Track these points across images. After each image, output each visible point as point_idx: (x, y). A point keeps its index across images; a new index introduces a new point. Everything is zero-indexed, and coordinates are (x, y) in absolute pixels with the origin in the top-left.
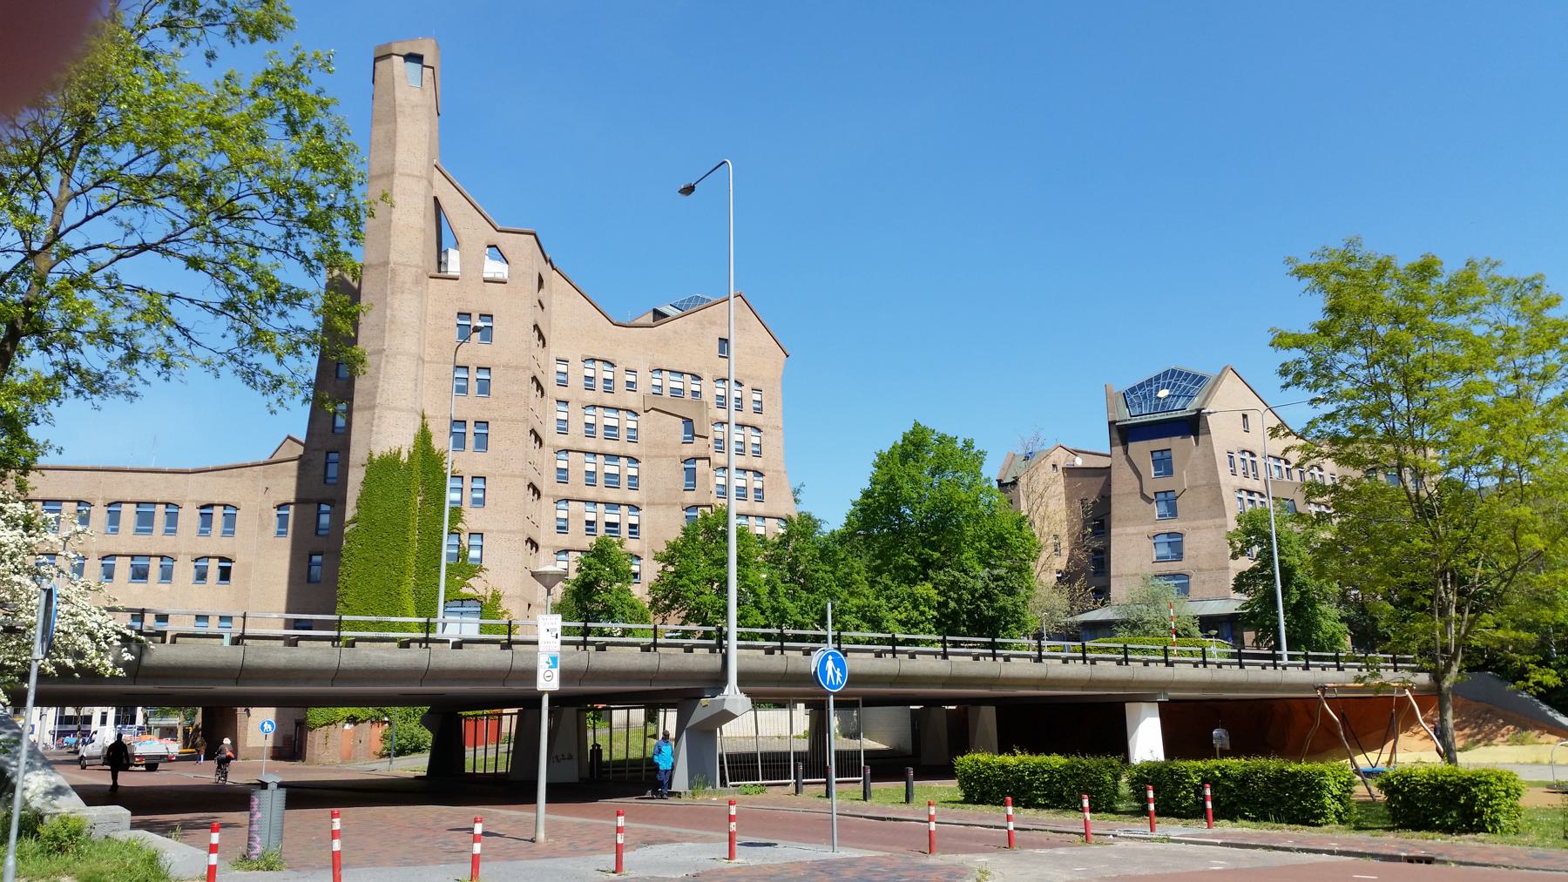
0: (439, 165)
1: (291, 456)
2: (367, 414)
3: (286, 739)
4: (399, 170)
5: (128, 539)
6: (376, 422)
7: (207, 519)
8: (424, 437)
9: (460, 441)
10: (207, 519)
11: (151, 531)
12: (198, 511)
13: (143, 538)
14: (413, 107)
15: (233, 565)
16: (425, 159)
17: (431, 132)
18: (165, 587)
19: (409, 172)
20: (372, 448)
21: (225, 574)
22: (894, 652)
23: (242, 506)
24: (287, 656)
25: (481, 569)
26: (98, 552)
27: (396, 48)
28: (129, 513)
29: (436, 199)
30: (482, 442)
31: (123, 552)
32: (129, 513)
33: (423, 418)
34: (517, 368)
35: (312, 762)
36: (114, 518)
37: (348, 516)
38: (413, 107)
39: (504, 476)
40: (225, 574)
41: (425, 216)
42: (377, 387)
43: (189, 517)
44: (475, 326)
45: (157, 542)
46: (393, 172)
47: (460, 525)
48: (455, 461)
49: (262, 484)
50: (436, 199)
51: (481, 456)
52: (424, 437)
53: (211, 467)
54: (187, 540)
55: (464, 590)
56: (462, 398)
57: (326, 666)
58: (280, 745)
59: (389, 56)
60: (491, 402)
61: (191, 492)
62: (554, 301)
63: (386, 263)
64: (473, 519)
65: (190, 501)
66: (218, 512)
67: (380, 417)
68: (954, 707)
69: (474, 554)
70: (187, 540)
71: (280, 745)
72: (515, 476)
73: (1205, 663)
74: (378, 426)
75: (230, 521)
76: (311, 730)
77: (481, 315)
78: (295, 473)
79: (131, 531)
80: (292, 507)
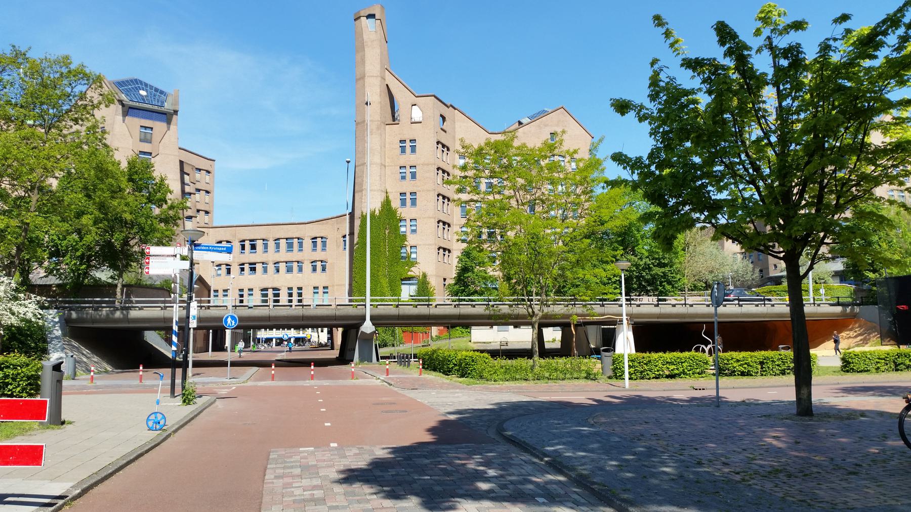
0: (388, 68)
2: (360, 193)
4: (367, 75)
5: (284, 255)
6: (363, 198)
7: (315, 244)
8: (387, 203)
9: (403, 203)
10: (315, 244)
11: (293, 250)
12: (239, 243)
13: (290, 253)
14: (372, 42)
15: (231, 267)
16: (378, 67)
17: (381, 52)
18: (300, 275)
19: (372, 75)
20: (363, 209)
21: (324, 269)
22: (765, 304)
23: (329, 237)
25: (416, 263)
26: (238, 263)
27: (362, 14)
28: (283, 243)
29: (387, 85)
30: (414, 202)
31: (259, 261)
32: (283, 243)
33: (387, 193)
34: (428, 165)
36: (278, 246)
37: (355, 242)
38: (372, 42)
39: (425, 218)
40: (324, 269)
41: (380, 95)
42: (363, 181)
43: (308, 243)
44: (408, 145)
45: (295, 255)
46: (364, 76)
47: (406, 243)
48: (406, 212)
49: (336, 227)
50: (387, 85)
51: (413, 209)
52: (387, 203)
53: (314, 220)
54: (307, 254)
55: (409, 273)
56: (404, 182)
59: (359, 17)
60: (417, 182)
61: (308, 232)
62: (456, 126)
63: (364, 121)
64: (411, 240)
66: (319, 240)
67: (365, 195)
69: (413, 256)
70: (307, 254)
72: (430, 218)
73: (685, 304)
74: (365, 199)
75: (324, 244)
77: (410, 140)
79: (285, 251)
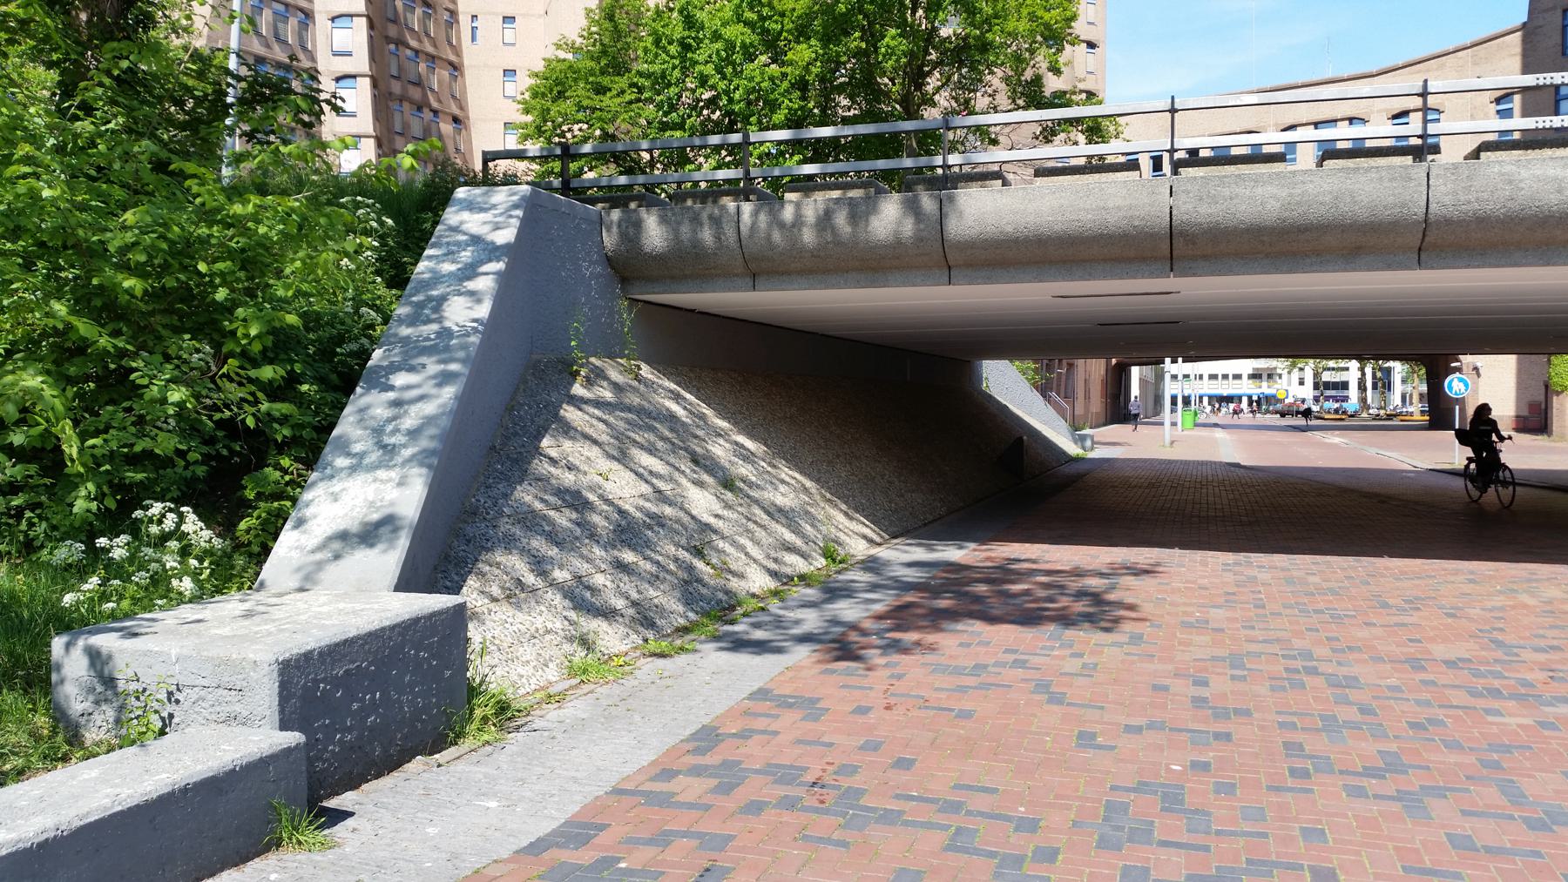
1: (1509, 26)
3: (1533, 407)
24: (1284, 193)
35: (1562, 438)
53: (1400, 63)
57: (1386, 214)
58: (1525, 413)
65: (1378, 111)
68: (1482, 428)
71: (1525, 413)
76: (1558, 394)
78: (1518, 49)
80: (1517, 98)
